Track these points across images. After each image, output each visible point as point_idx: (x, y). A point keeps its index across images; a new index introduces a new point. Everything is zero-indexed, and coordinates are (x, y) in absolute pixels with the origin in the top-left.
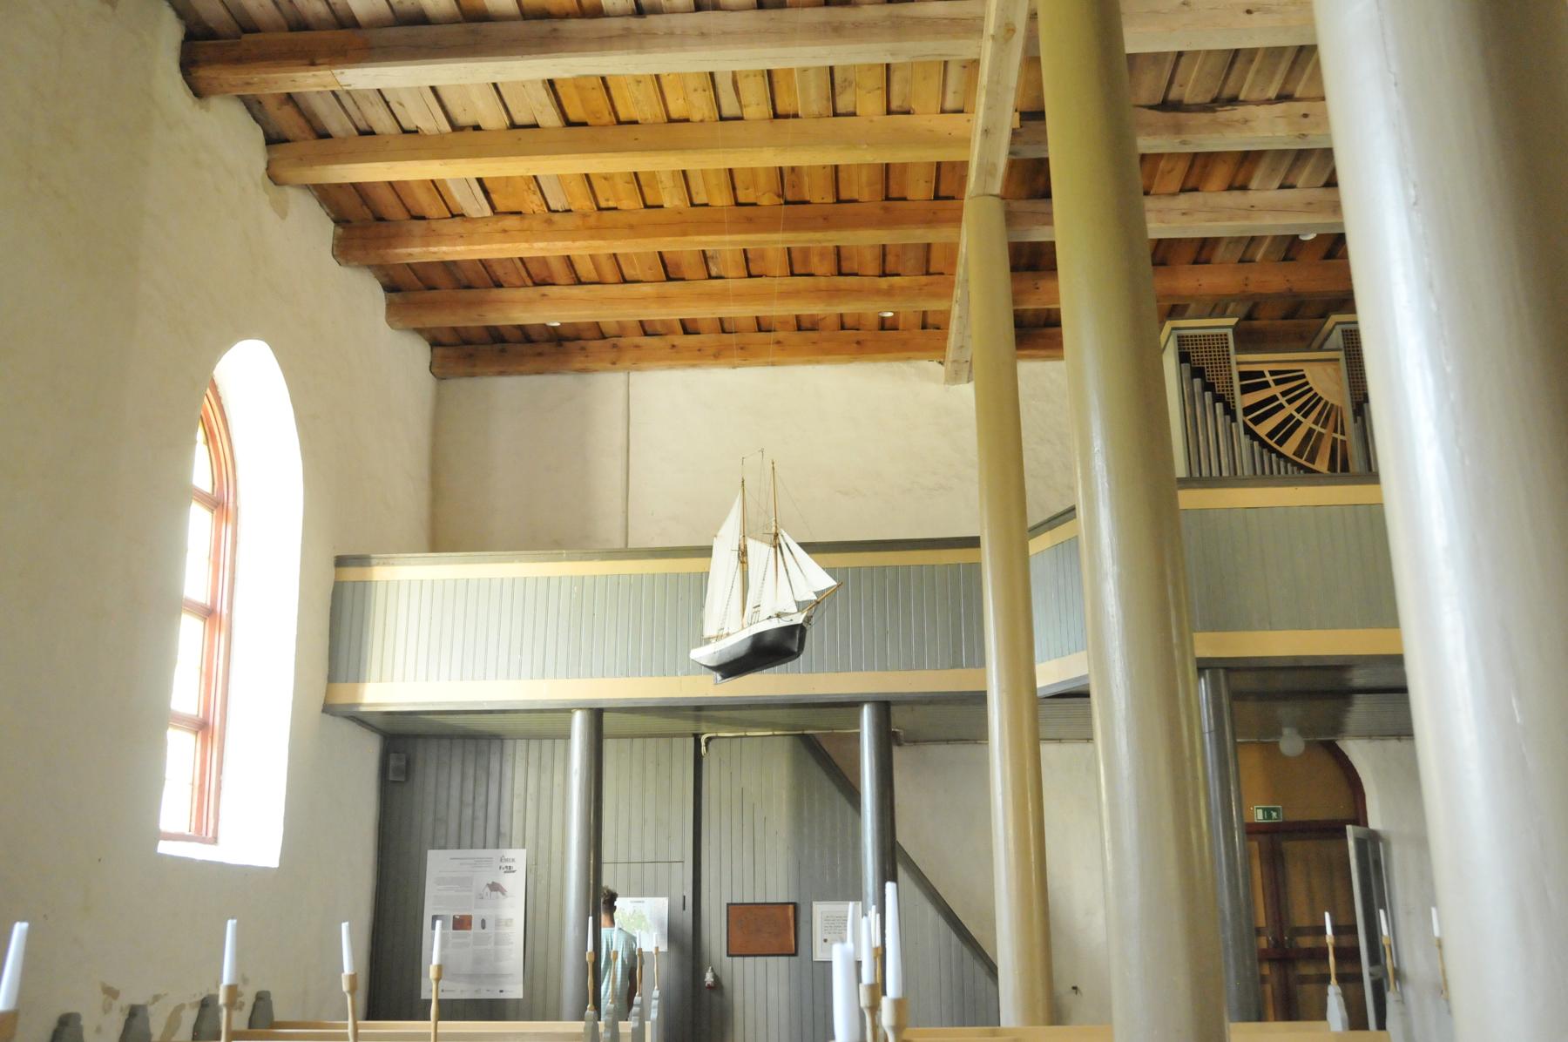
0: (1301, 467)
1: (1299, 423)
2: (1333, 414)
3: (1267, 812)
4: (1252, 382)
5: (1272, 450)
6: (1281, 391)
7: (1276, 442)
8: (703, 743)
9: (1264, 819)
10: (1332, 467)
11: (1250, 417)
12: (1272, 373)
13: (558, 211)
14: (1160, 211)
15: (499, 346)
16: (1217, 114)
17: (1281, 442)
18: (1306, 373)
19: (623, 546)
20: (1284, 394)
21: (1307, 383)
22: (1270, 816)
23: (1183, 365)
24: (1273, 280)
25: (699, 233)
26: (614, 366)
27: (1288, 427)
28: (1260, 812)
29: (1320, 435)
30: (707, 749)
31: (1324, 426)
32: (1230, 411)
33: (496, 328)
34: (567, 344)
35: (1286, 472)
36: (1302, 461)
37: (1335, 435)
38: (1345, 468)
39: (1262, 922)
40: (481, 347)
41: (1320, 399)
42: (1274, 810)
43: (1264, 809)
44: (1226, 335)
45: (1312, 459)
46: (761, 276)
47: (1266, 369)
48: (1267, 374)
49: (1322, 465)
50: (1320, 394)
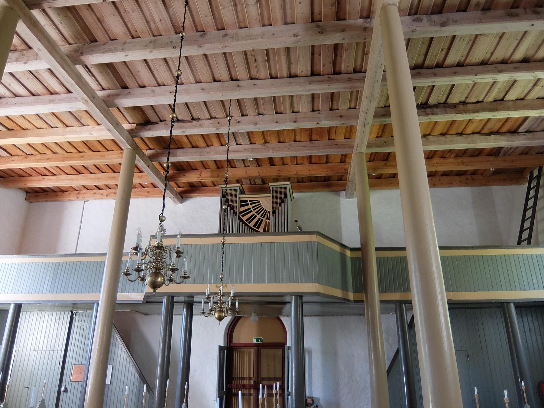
0: (254, 230)
1: (256, 216)
2: (267, 214)
3: (258, 339)
4: (243, 203)
5: (246, 224)
6: (252, 206)
7: (248, 223)
8: (74, 314)
9: (256, 342)
10: (264, 230)
11: (241, 215)
12: (250, 201)
13: (29, 155)
14: (200, 152)
15: (46, 193)
16: (193, 123)
17: (249, 223)
18: (260, 201)
19: (74, 253)
20: (253, 207)
21: (260, 204)
22: (258, 341)
23: (222, 199)
24: (254, 172)
25: (67, 161)
26: (78, 199)
27: (253, 217)
28: (255, 339)
29: (262, 220)
30: (75, 316)
31: (264, 217)
32: (234, 213)
33: (191, 183)
34: (64, 192)
35: (251, 232)
36: (255, 228)
37: (266, 220)
38: (268, 231)
39: (252, 376)
40: (72, 192)
41: (264, 209)
42: (260, 339)
43: (256, 339)
44: (237, 189)
45: (258, 228)
46: (106, 173)
47: (248, 200)
48: (249, 201)
49: (261, 230)
50: (264, 207)
